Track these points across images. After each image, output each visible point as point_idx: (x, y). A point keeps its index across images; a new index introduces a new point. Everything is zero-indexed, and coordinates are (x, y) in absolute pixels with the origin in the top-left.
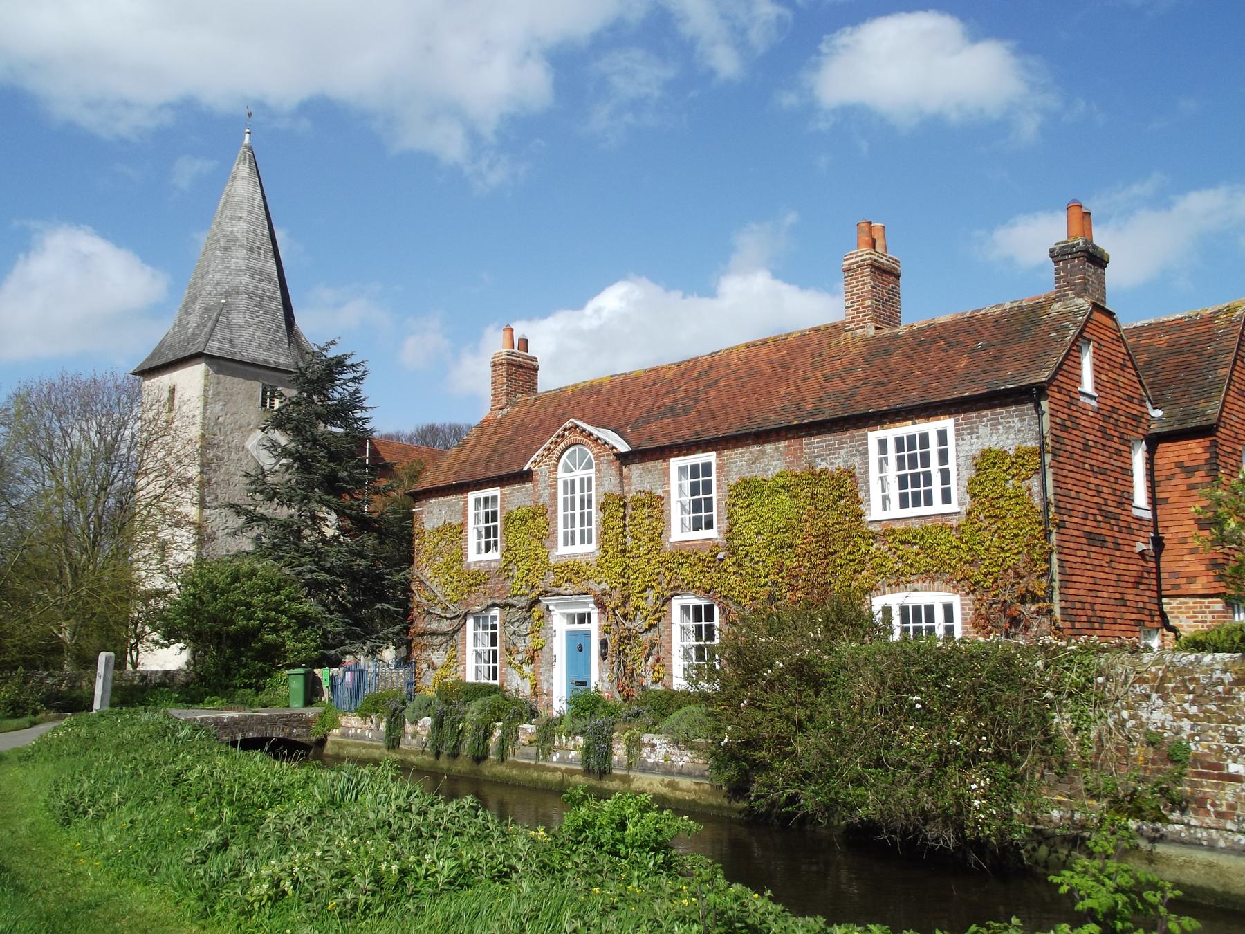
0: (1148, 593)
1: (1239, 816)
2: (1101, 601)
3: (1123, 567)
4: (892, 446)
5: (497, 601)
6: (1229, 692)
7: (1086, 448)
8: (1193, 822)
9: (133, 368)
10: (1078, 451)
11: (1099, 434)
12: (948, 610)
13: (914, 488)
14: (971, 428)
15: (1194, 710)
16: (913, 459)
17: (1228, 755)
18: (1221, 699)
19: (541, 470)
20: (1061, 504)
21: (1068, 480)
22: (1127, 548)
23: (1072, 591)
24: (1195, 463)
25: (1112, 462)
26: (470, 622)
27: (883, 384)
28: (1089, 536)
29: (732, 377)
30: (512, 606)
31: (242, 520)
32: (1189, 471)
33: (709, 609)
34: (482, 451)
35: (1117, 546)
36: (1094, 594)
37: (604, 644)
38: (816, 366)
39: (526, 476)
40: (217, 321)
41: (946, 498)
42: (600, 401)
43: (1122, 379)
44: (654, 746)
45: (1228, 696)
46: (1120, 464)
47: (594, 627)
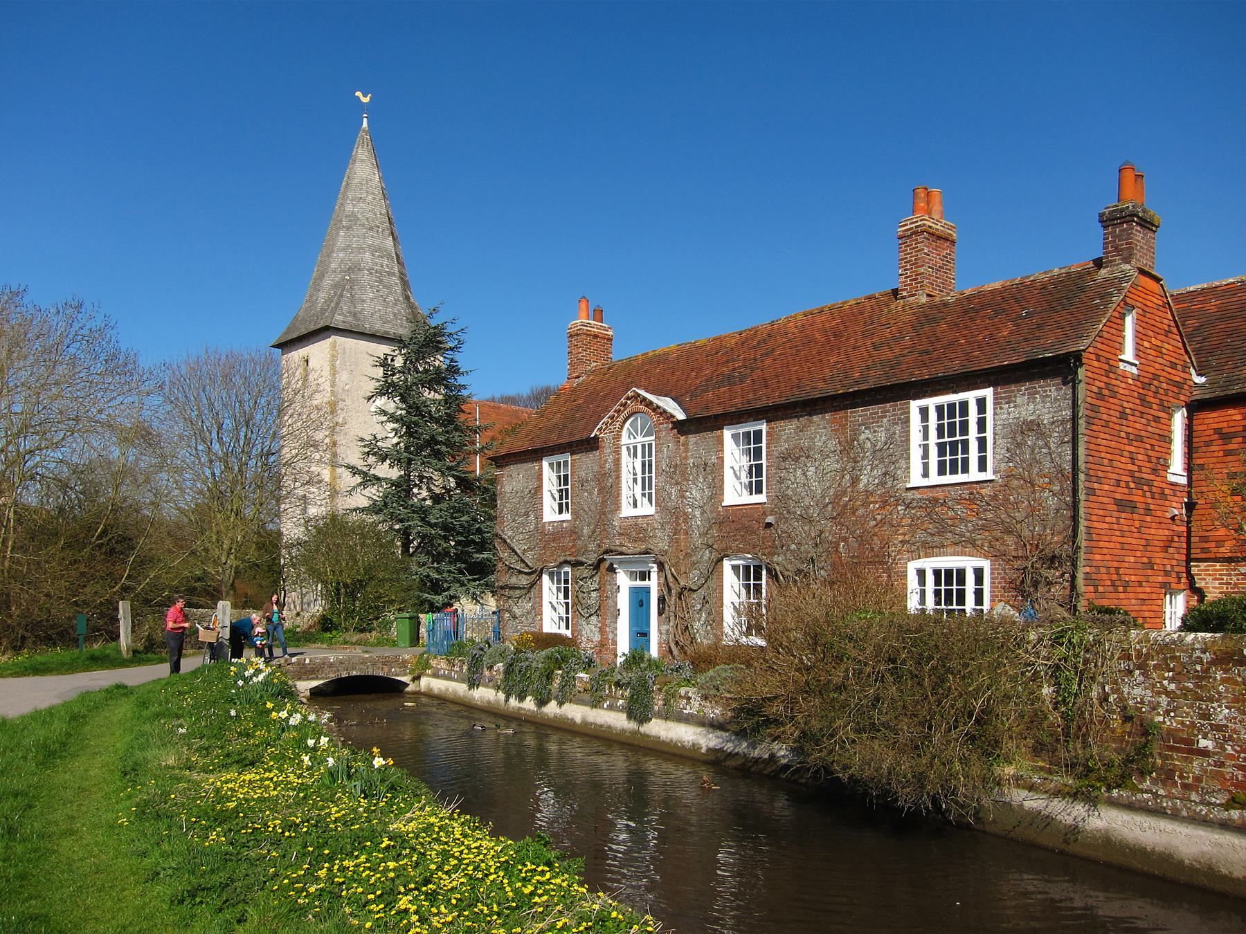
0: (1176, 556)
1: (1203, 788)
2: (1127, 565)
3: (1153, 531)
4: (933, 415)
5: (569, 558)
6: (1206, 671)
7: (1123, 415)
8: (1161, 792)
9: (273, 342)
10: (1114, 419)
11: (1138, 402)
12: (979, 573)
13: (952, 455)
14: (1010, 397)
15: (1172, 687)
16: (952, 426)
17: (1199, 730)
18: (1198, 677)
19: (606, 437)
20: (1091, 473)
21: (1102, 448)
22: (1159, 513)
23: (1097, 557)
24: (1232, 430)
25: (1150, 429)
26: (545, 578)
27: (928, 352)
28: (1122, 505)
29: (787, 345)
30: (582, 564)
31: (358, 479)
32: (1225, 437)
33: (758, 570)
34: (557, 418)
35: (1148, 511)
36: (1121, 558)
37: (662, 600)
38: (868, 334)
39: (591, 444)
40: (342, 295)
41: (982, 466)
42: (661, 372)
43: (1166, 346)
44: (689, 698)
45: (1205, 675)
46: (1158, 431)
47: (653, 583)
